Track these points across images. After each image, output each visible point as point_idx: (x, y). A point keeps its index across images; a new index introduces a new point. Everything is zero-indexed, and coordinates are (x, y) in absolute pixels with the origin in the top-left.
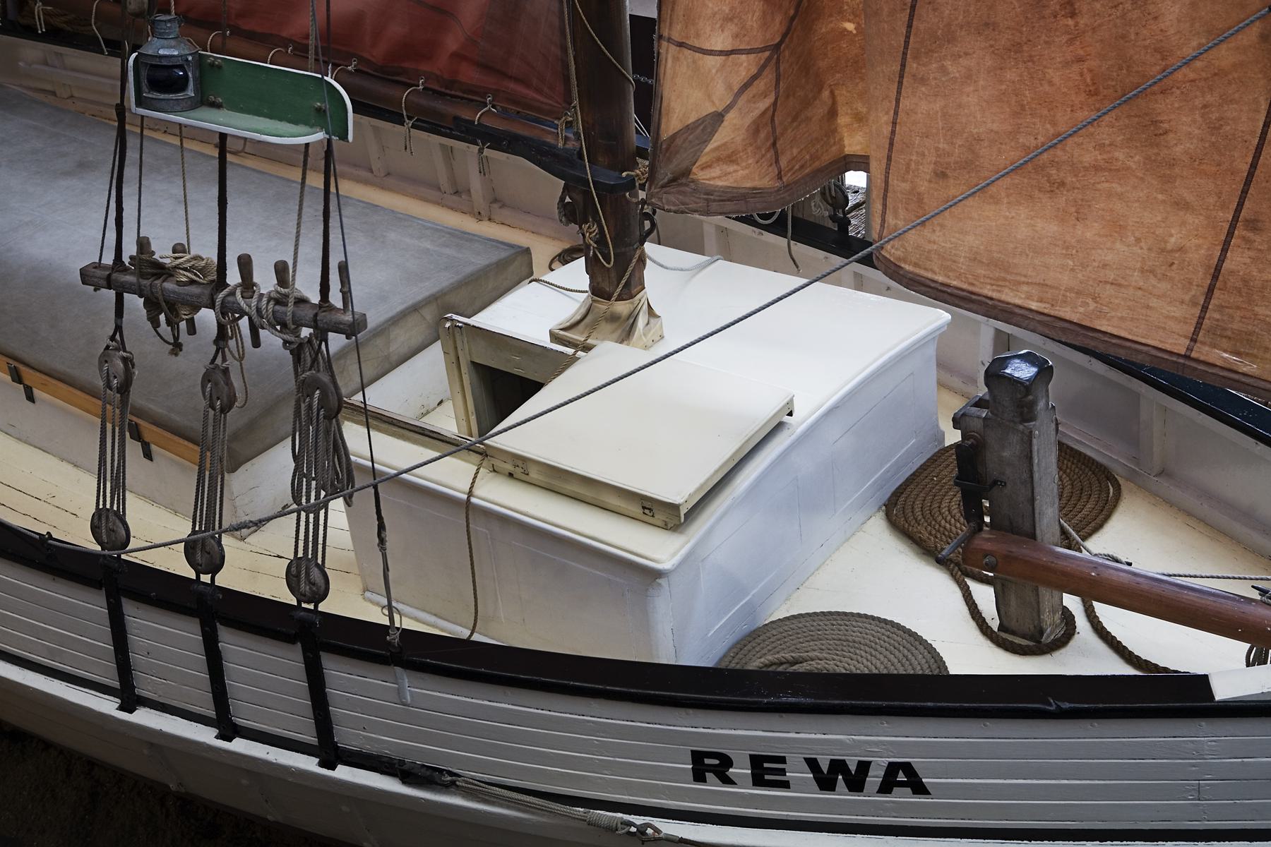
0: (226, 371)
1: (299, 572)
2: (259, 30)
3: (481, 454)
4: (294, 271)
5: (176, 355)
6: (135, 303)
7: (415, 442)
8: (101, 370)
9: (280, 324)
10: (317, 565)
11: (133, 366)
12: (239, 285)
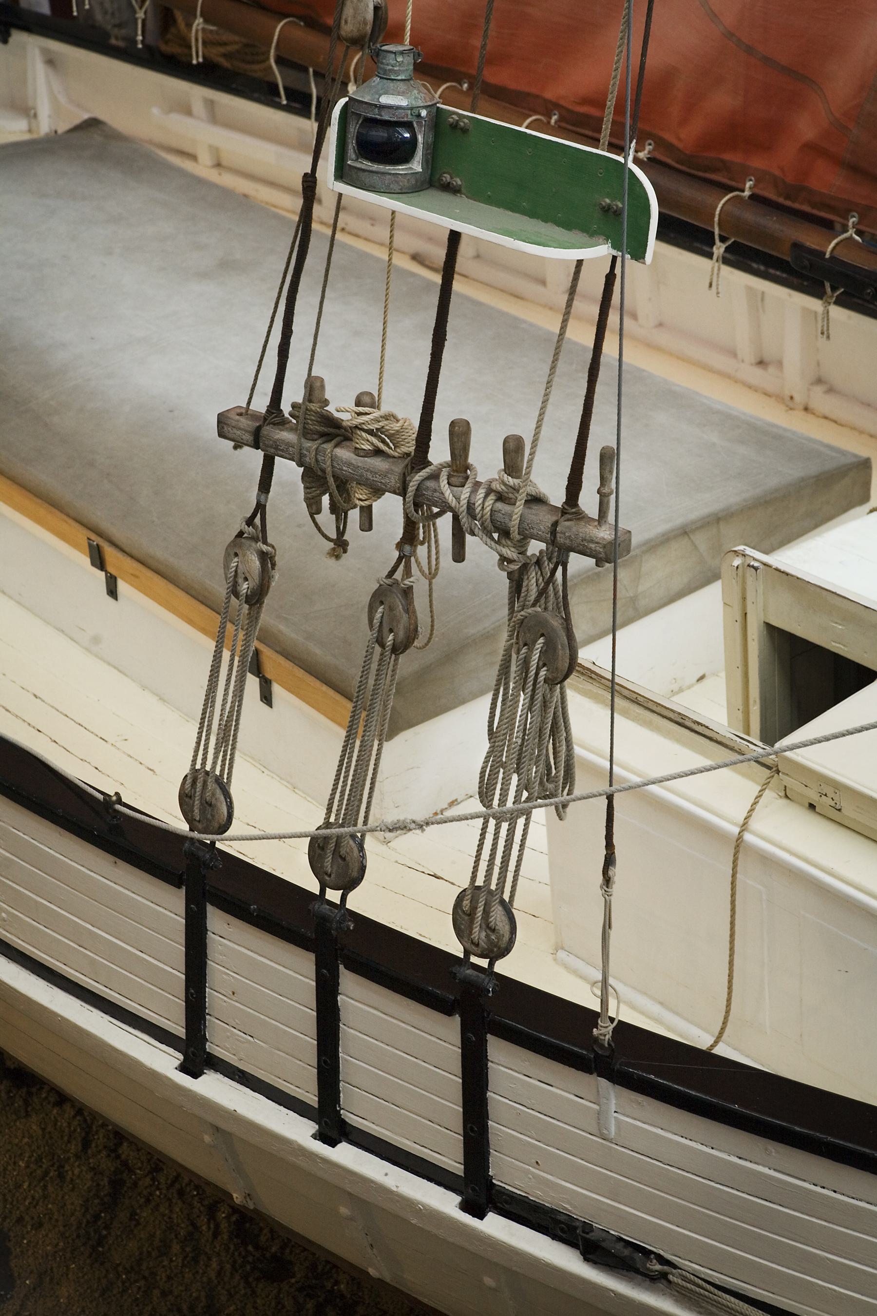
0: (407, 592)
1: (474, 909)
2: (512, 85)
3: (769, 768)
4: (532, 454)
5: (338, 557)
6: (287, 471)
7: (667, 735)
8: (226, 567)
9: (498, 530)
10: (502, 902)
11: (274, 565)
12: (448, 465)
